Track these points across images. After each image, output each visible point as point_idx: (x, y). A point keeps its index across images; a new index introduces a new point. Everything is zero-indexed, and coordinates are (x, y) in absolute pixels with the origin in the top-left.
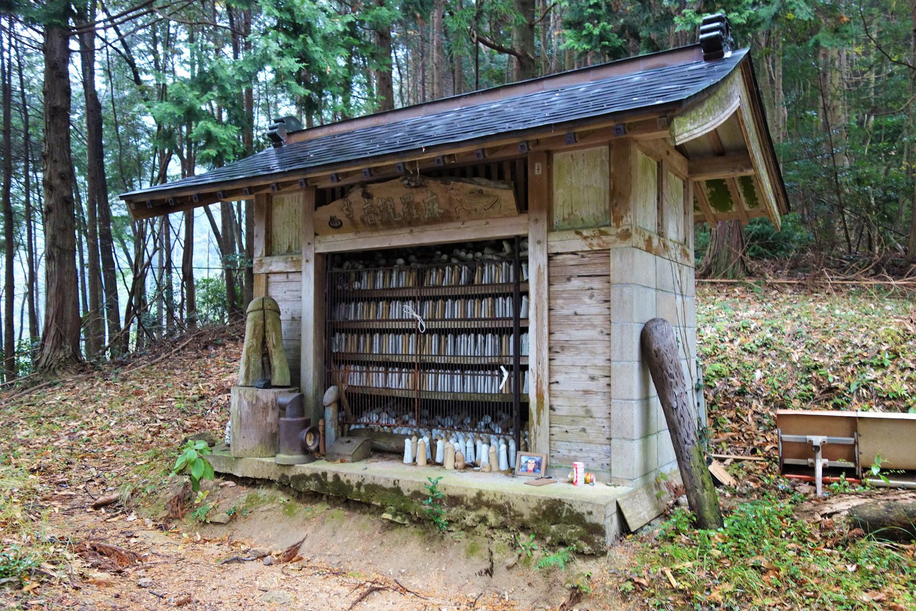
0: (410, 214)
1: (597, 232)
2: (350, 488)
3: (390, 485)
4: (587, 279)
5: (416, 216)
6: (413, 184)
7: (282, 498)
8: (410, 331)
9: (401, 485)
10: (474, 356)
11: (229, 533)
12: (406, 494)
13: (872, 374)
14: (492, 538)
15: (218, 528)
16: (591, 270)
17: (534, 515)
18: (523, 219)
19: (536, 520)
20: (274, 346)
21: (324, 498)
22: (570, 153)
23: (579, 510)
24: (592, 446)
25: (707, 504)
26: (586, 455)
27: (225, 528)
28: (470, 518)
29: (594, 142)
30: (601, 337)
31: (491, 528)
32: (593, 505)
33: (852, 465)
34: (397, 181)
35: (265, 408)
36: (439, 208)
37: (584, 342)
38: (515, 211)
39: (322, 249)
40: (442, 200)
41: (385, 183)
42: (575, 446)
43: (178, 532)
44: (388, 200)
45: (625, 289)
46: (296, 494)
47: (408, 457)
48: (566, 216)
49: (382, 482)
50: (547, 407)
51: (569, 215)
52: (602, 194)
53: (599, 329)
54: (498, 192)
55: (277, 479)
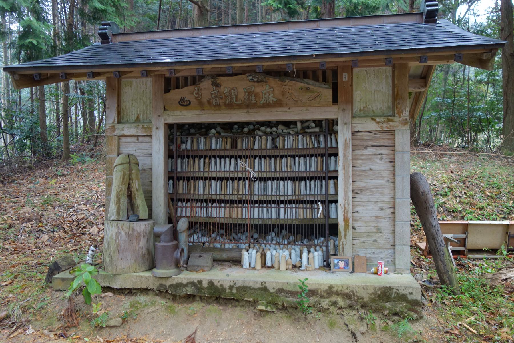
0: (249, 99)
1: (386, 119)
2: (223, 290)
3: (258, 286)
4: (378, 148)
5: (253, 102)
6: (256, 80)
7: (161, 301)
8: (244, 179)
9: (267, 285)
10: (272, 195)
11: (125, 333)
12: (271, 291)
13: (442, 200)
14: (342, 315)
15: (113, 330)
16: (381, 143)
17: (372, 298)
18: (334, 108)
19: (374, 301)
20: (137, 190)
21: (198, 298)
22: (365, 69)
23: (403, 292)
24: (381, 250)
25: (455, 280)
26: (377, 256)
27: (120, 329)
28: (325, 303)
29: (375, 64)
30: (387, 184)
31: (340, 308)
32: (413, 288)
33: (462, 248)
34: (243, 76)
35: (139, 236)
36: (273, 97)
37: (376, 187)
38: (331, 103)
39: (171, 120)
40: (276, 92)
41: (234, 77)
42: (369, 251)
43: (79, 338)
44: (233, 89)
45: (405, 155)
46: (172, 297)
47: (246, 263)
48: (362, 108)
49: (251, 284)
50: (351, 227)
51: (364, 107)
52: (387, 97)
53: (386, 179)
54: (321, 90)
55: (155, 288)
